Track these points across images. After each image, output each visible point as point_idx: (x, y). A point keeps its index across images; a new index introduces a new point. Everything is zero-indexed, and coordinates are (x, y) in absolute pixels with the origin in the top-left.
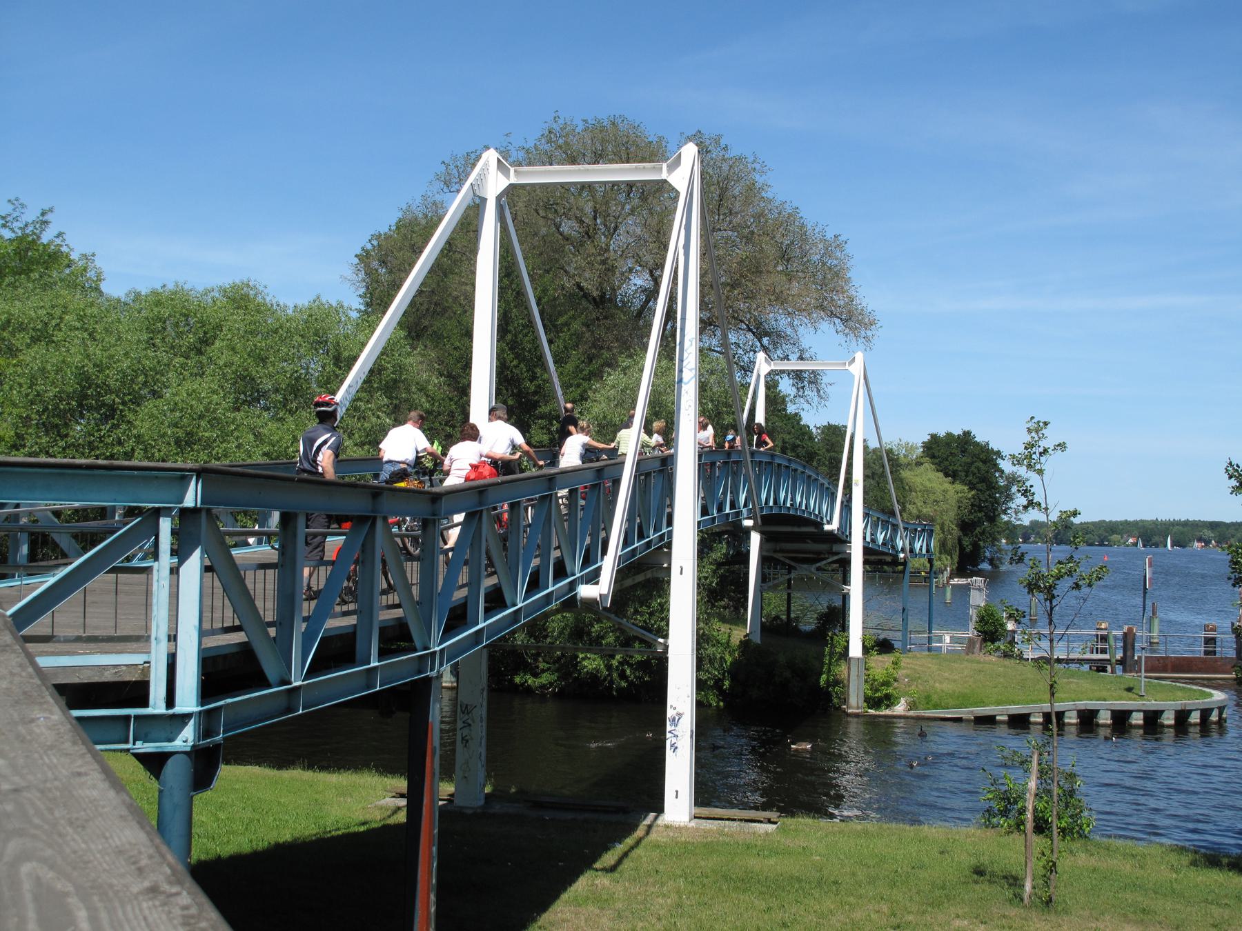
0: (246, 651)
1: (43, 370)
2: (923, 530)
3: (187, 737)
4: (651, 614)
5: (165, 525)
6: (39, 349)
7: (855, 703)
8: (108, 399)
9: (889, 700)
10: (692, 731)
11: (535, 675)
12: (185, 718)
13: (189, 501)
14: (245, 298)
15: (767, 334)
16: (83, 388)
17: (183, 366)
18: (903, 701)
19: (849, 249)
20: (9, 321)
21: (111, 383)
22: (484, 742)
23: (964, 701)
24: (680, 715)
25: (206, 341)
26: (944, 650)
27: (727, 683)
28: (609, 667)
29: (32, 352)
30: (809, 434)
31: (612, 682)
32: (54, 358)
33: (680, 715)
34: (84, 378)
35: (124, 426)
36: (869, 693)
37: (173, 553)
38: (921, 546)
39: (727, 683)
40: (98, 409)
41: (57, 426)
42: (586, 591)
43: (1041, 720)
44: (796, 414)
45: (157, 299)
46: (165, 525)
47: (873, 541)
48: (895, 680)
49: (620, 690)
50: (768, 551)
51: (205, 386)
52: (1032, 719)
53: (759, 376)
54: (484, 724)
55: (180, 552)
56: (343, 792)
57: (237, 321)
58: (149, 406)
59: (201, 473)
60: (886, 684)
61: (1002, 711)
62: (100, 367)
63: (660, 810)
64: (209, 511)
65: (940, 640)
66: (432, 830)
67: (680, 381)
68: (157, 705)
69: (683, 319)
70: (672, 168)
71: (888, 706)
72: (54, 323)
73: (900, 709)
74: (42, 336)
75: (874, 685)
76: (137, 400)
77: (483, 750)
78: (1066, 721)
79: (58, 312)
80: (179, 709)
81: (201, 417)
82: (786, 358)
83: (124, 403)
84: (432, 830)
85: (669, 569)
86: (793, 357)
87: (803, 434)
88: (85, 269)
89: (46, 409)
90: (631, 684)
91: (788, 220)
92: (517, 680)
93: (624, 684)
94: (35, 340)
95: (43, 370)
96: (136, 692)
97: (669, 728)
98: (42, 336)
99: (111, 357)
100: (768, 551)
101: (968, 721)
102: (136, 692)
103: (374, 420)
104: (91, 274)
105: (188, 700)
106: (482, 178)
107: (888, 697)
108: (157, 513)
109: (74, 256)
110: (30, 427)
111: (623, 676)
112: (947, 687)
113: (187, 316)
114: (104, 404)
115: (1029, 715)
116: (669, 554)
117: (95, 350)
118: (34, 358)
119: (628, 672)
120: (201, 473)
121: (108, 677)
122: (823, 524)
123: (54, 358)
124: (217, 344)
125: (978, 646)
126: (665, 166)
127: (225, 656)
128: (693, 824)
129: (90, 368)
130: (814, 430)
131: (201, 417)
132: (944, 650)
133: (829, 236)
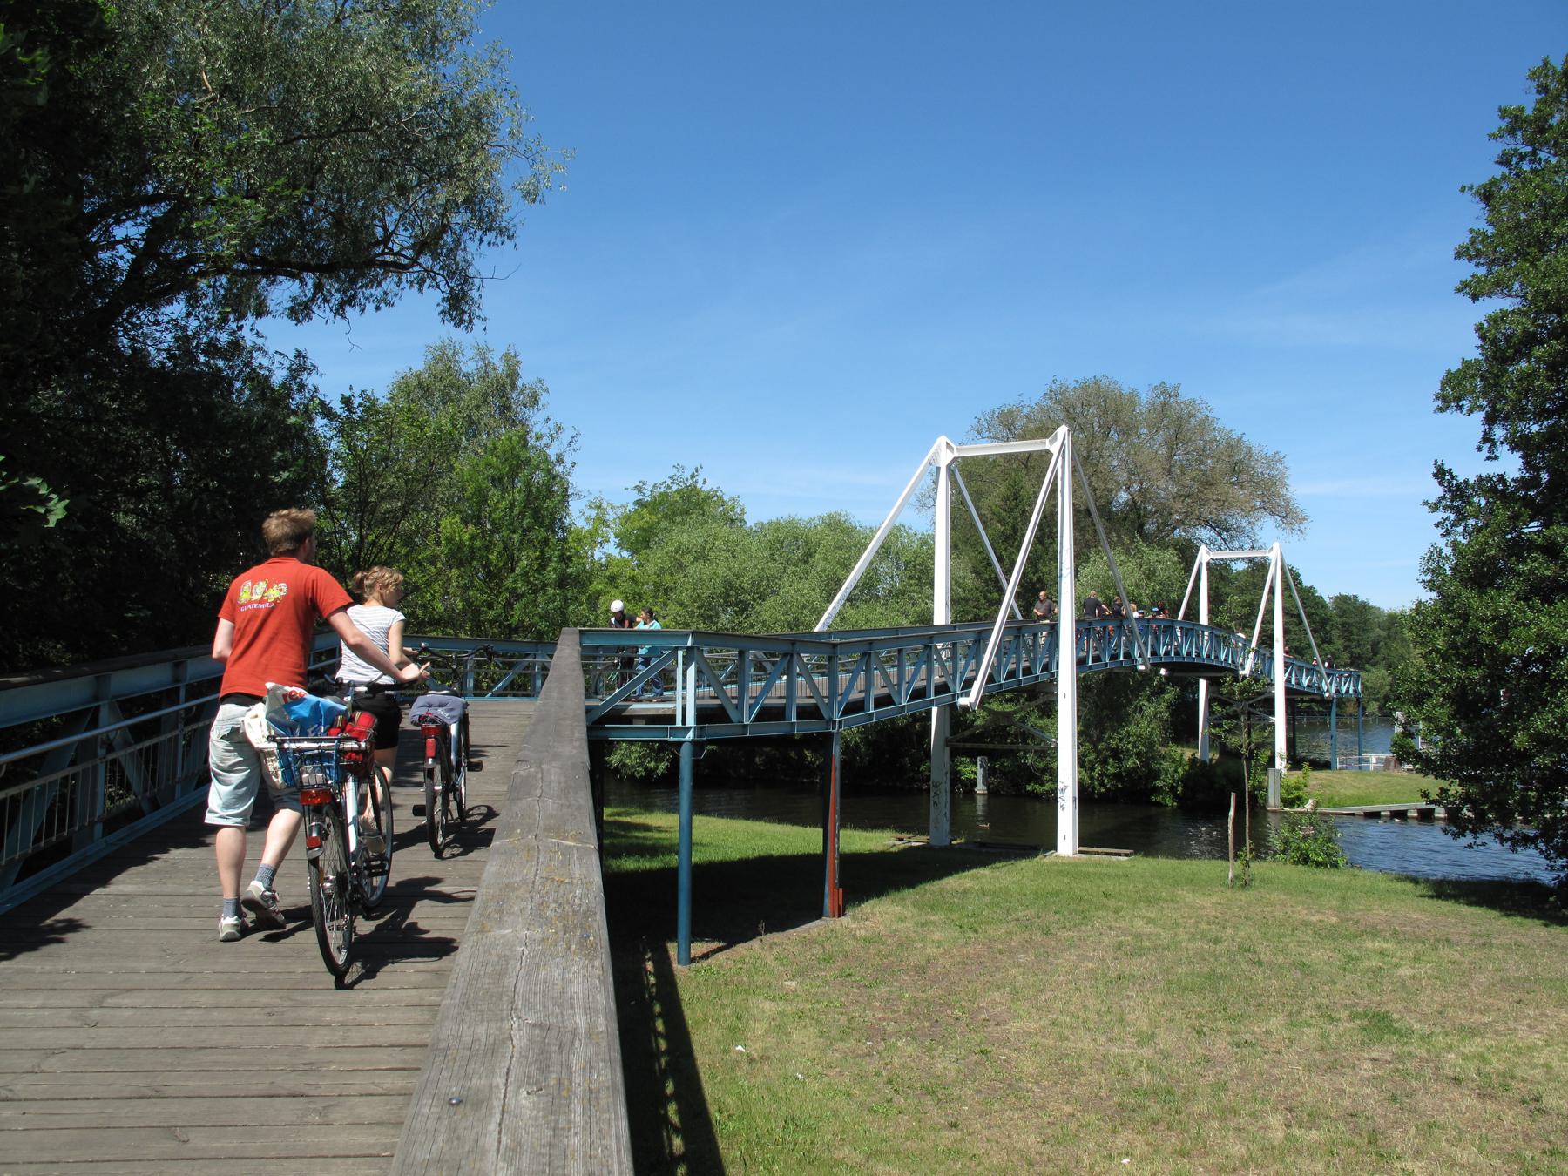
0: (721, 708)
1: (701, 579)
2: (1350, 676)
3: (690, 736)
4: (1121, 740)
5: (680, 653)
6: (700, 564)
7: (1273, 801)
8: (742, 597)
9: (1299, 801)
10: (1074, 798)
11: (1042, 784)
12: (690, 728)
13: (689, 644)
14: (838, 523)
15: (1225, 529)
16: (727, 590)
17: (794, 573)
18: (1310, 801)
19: (1287, 462)
20: (680, 547)
21: (745, 586)
22: (948, 805)
23: (1359, 800)
24: (1066, 787)
25: (810, 555)
26: (1372, 768)
27: (1180, 789)
28: (1092, 778)
29: (694, 567)
30: (1324, 606)
31: (1094, 789)
32: (708, 571)
33: (1066, 787)
34: (729, 585)
35: (754, 615)
36: (1285, 795)
37: (683, 664)
38: (1348, 688)
39: (1180, 789)
40: (737, 605)
41: (711, 616)
42: (963, 701)
43: (1416, 815)
44: (1311, 587)
45: (776, 527)
46: (680, 653)
47: (1298, 683)
48: (1306, 786)
49: (1100, 794)
50: (1213, 692)
51: (805, 586)
52: (1409, 814)
53: (1201, 564)
54: (948, 794)
55: (686, 665)
56: (866, 839)
57: (830, 539)
58: (770, 602)
59: (693, 633)
60: (1298, 789)
61: (1385, 809)
62: (738, 577)
63: (1054, 848)
64: (698, 648)
65: (1368, 761)
66: (835, 806)
67: (1061, 576)
68: (679, 723)
69: (1062, 537)
70: (1052, 442)
71: (1299, 806)
72: (708, 547)
73: (1308, 806)
74: (701, 556)
75: (1288, 790)
76: (762, 597)
77: (947, 811)
78: (1436, 815)
79: (711, 539)
80: (687, 725)
81: (804, 607)
82: (1241, 547)
83: (754, 600)
84: (835, 806)
85: (1057, 694)
86: (1247, 546)
87: (1317, 603)
88: (734, 507)
89: (703, 605)
90: (1108, 790)
91: (1233, 446)
92: (1029, 788)
93: (1103, 790)
94: (696, 559)
95: (701, 579)
96: (671, 718)
97: (1059, 795)
98: (701, 556)
99: (745, 569)
100: (1213, 692)
101: (1360, 815)
102: (671, 718)
103: (923, 605)
104: (738, 510)
105: (691, 721)
106: (936, 455)
107: (1299, 798)
108: (677, 649)
109: (726, 498)
110: (693, 618)
111: (1102, 784)
112: (1349, 792)
113: (797, 539)
114: (741, 601)
115: (1406, 811)
116: (1057, 685)
117: (735, 566)
118: (695, 572)
119: (1106, 781)
120: (693, 633)
121: (660, 713)
122: (1238, 670)
123: (708, 571)
124: (817, 556)
125: (1392, 764)
126: (1047, 440)
127: (711, 709)
128: (1078, 856)
129: (731, 577)
130: (1327, 600)
131: (804, 607)
132: (1372, 768)
133: (1271, 453)
